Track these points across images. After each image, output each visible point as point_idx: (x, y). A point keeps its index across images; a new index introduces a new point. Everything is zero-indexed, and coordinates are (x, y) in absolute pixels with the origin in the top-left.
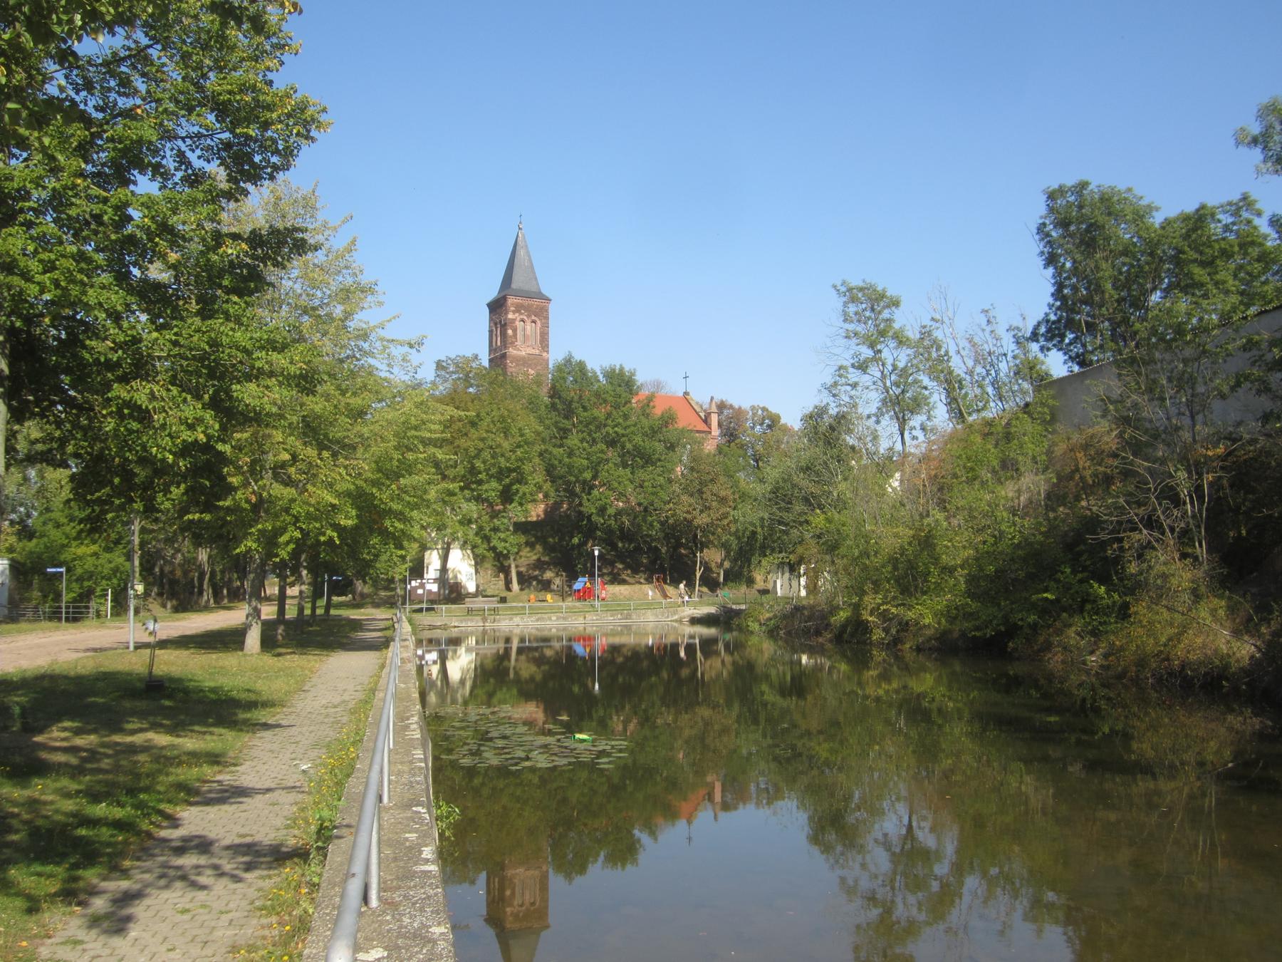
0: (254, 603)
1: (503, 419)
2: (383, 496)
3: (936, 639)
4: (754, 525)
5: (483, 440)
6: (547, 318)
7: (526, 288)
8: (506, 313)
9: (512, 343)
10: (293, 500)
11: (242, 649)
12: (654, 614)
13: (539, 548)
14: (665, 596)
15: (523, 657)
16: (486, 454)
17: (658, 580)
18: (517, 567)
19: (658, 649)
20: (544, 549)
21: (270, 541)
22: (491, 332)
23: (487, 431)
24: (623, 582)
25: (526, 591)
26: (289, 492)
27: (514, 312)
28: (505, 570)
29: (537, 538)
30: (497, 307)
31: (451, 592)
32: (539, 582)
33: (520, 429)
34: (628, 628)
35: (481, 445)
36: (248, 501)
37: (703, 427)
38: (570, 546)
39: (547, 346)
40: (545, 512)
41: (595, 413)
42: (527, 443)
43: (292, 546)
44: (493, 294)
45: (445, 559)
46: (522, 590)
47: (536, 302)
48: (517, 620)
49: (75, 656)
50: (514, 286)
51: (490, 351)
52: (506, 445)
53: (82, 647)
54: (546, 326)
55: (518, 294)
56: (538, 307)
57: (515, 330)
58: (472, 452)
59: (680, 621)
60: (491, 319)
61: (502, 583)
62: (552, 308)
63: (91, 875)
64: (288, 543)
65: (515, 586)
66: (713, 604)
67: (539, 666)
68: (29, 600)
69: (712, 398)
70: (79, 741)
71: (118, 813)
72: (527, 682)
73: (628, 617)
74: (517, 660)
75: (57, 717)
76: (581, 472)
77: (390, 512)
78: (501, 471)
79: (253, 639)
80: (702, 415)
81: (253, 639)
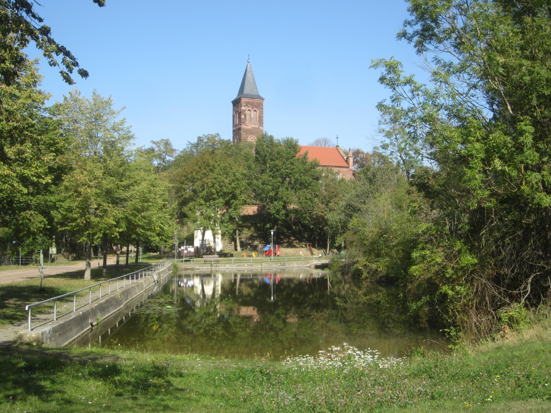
0: (88, 261)
1: (225, 168)
2: (136, 220)
3: (384, 277)
4: (336, 222)
5: (215, 179)
6: (262, 109)
7: (251, 93)
8: (241, 107)
9: (244, 122)
10: (99, 222)
11: (83, 278)
12: (300, 262)
13: (252, 229)
14: (312, 254)
15: (243, 284)
16: (217, 186)
17: (309, 245)
18: (240, 238)
19: (309, 280)
20: (255, 230)
21: (91, 237)
22: (234, 116)
23: (218, 174)
24: (294, 246)
25: (245, 250)
26: (98, 219)
27: (245, 106)
28: (234, 240)
29: (251, 223)
30: (236, 103)
31: (207, 251)
32: (251, 246)
33: (234, 173)
34: (284, 270)
35: (215, 181)
36: (82, 223)
37: (345, 164)
38: (271, 228)
39: (262, 123)
40: (258, 210)
41: (278, 162)
42: (237, 179)
43: (99, 240)
44: (235, 96)
45: (203, 234)
46: (243, 250)
47: (256, 101)
48: (228, 266)
49: (21, 280)
50: (245, 92)
51: (233, 126)
52: (227, 181)
53: (25, 277)
54: (261, 113)
55: (247, 96)
56: (257, 102)
57: (245, 116)
58: (210, 184)
59: (310, 267)
60: (234, 110)
61: (233, 247)
62: (265, 104)
63: (14, 321)
64: (98, 238)
65: (239, 248)
66: (327, 259)
67: (252, 288)
68: (6, 255)
69: (350, 149)
70: (18, 303)
71: (22, 314)
72: (246, 296)
73: (284, 265)
74: (240, 285)
75: (12, 298)
76: (268, 192)
77: (139, 225)
78: (225, 193)
79: (88, 275)
80: (345, 158)
81: (88, 275)
